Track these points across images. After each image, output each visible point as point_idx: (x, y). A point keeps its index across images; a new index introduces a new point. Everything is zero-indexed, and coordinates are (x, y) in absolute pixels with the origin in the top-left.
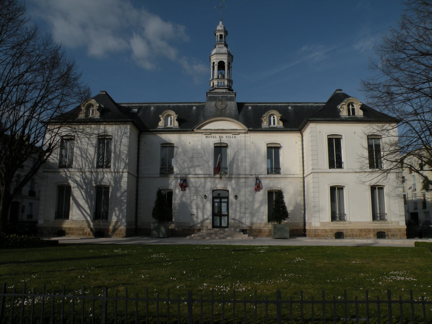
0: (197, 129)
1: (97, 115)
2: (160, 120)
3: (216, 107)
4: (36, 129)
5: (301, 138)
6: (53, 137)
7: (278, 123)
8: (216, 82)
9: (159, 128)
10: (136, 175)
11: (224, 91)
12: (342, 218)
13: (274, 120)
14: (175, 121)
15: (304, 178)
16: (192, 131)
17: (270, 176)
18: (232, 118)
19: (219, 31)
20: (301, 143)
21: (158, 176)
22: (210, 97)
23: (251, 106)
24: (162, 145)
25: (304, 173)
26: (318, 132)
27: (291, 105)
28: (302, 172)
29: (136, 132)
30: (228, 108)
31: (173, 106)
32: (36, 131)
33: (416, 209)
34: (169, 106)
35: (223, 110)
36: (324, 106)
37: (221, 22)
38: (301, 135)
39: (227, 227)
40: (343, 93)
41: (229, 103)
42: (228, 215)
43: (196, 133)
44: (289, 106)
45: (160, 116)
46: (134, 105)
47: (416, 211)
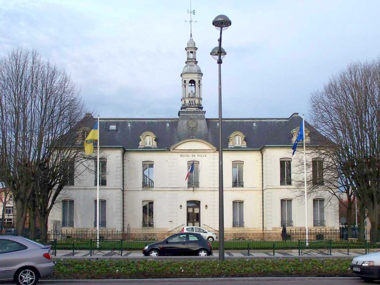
3: (188, 125)
5: (261, 156)
7: (242, 143)
9: (140, 148)
10: (122, 189)
11: (195, 109)
12: (241, 224)
13: (239, 140)
15: (263, 190)
16: (168, 150)
17: (235, 189)
18: (202, 139)
20: (261, 160)
21: (141, 189)
22: (182, 115)
24: (143, 163)
25: (263, 187)
26: (275, 155)
28: (261, 185)
30: (198, 126)
35: (194, 129)
38: (261, 154)
40: (299, 117)
41: (199, 121)
44: (253, 122)
45: (140, 137)
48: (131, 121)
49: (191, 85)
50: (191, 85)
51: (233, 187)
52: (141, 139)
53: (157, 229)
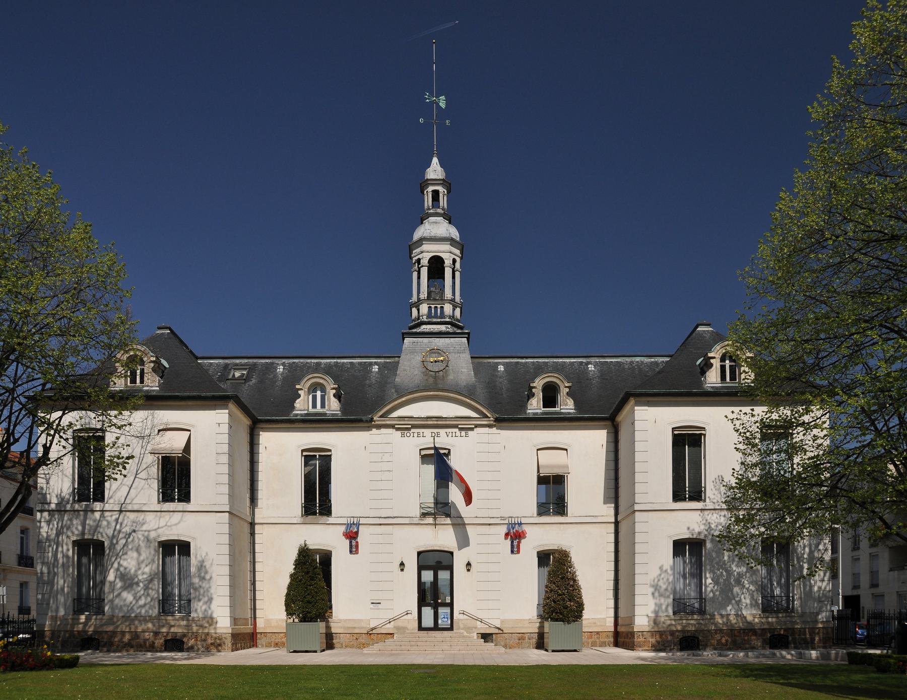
0: (381, 417)
1: (152, 383)
2: (299, 396)
4: (11, 413)
6: (17, 414)
8: (424, 308)
9: (297, 415)
11: (443, 328)
14: (333, 399)
19: (435, 182)
23: (503, 364)
27: (593, 360)
29: (246, 422)
31: (326, 364)
32: (9, 417)
33: (856, 587)
34: (318, 364)
36: (667, 362)
37: (435, 160)
39: (451, 628)
42: (451, 605)
43: (379, 427)
46: (238, 361)
47: (855, 593)
48: (286, 361)
49: (448, 610)
50: (448, 610)
51: (540, 514)
52: (300, 392)
53: (340, 621)
